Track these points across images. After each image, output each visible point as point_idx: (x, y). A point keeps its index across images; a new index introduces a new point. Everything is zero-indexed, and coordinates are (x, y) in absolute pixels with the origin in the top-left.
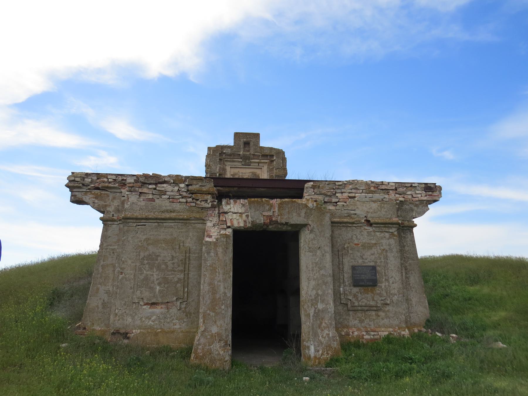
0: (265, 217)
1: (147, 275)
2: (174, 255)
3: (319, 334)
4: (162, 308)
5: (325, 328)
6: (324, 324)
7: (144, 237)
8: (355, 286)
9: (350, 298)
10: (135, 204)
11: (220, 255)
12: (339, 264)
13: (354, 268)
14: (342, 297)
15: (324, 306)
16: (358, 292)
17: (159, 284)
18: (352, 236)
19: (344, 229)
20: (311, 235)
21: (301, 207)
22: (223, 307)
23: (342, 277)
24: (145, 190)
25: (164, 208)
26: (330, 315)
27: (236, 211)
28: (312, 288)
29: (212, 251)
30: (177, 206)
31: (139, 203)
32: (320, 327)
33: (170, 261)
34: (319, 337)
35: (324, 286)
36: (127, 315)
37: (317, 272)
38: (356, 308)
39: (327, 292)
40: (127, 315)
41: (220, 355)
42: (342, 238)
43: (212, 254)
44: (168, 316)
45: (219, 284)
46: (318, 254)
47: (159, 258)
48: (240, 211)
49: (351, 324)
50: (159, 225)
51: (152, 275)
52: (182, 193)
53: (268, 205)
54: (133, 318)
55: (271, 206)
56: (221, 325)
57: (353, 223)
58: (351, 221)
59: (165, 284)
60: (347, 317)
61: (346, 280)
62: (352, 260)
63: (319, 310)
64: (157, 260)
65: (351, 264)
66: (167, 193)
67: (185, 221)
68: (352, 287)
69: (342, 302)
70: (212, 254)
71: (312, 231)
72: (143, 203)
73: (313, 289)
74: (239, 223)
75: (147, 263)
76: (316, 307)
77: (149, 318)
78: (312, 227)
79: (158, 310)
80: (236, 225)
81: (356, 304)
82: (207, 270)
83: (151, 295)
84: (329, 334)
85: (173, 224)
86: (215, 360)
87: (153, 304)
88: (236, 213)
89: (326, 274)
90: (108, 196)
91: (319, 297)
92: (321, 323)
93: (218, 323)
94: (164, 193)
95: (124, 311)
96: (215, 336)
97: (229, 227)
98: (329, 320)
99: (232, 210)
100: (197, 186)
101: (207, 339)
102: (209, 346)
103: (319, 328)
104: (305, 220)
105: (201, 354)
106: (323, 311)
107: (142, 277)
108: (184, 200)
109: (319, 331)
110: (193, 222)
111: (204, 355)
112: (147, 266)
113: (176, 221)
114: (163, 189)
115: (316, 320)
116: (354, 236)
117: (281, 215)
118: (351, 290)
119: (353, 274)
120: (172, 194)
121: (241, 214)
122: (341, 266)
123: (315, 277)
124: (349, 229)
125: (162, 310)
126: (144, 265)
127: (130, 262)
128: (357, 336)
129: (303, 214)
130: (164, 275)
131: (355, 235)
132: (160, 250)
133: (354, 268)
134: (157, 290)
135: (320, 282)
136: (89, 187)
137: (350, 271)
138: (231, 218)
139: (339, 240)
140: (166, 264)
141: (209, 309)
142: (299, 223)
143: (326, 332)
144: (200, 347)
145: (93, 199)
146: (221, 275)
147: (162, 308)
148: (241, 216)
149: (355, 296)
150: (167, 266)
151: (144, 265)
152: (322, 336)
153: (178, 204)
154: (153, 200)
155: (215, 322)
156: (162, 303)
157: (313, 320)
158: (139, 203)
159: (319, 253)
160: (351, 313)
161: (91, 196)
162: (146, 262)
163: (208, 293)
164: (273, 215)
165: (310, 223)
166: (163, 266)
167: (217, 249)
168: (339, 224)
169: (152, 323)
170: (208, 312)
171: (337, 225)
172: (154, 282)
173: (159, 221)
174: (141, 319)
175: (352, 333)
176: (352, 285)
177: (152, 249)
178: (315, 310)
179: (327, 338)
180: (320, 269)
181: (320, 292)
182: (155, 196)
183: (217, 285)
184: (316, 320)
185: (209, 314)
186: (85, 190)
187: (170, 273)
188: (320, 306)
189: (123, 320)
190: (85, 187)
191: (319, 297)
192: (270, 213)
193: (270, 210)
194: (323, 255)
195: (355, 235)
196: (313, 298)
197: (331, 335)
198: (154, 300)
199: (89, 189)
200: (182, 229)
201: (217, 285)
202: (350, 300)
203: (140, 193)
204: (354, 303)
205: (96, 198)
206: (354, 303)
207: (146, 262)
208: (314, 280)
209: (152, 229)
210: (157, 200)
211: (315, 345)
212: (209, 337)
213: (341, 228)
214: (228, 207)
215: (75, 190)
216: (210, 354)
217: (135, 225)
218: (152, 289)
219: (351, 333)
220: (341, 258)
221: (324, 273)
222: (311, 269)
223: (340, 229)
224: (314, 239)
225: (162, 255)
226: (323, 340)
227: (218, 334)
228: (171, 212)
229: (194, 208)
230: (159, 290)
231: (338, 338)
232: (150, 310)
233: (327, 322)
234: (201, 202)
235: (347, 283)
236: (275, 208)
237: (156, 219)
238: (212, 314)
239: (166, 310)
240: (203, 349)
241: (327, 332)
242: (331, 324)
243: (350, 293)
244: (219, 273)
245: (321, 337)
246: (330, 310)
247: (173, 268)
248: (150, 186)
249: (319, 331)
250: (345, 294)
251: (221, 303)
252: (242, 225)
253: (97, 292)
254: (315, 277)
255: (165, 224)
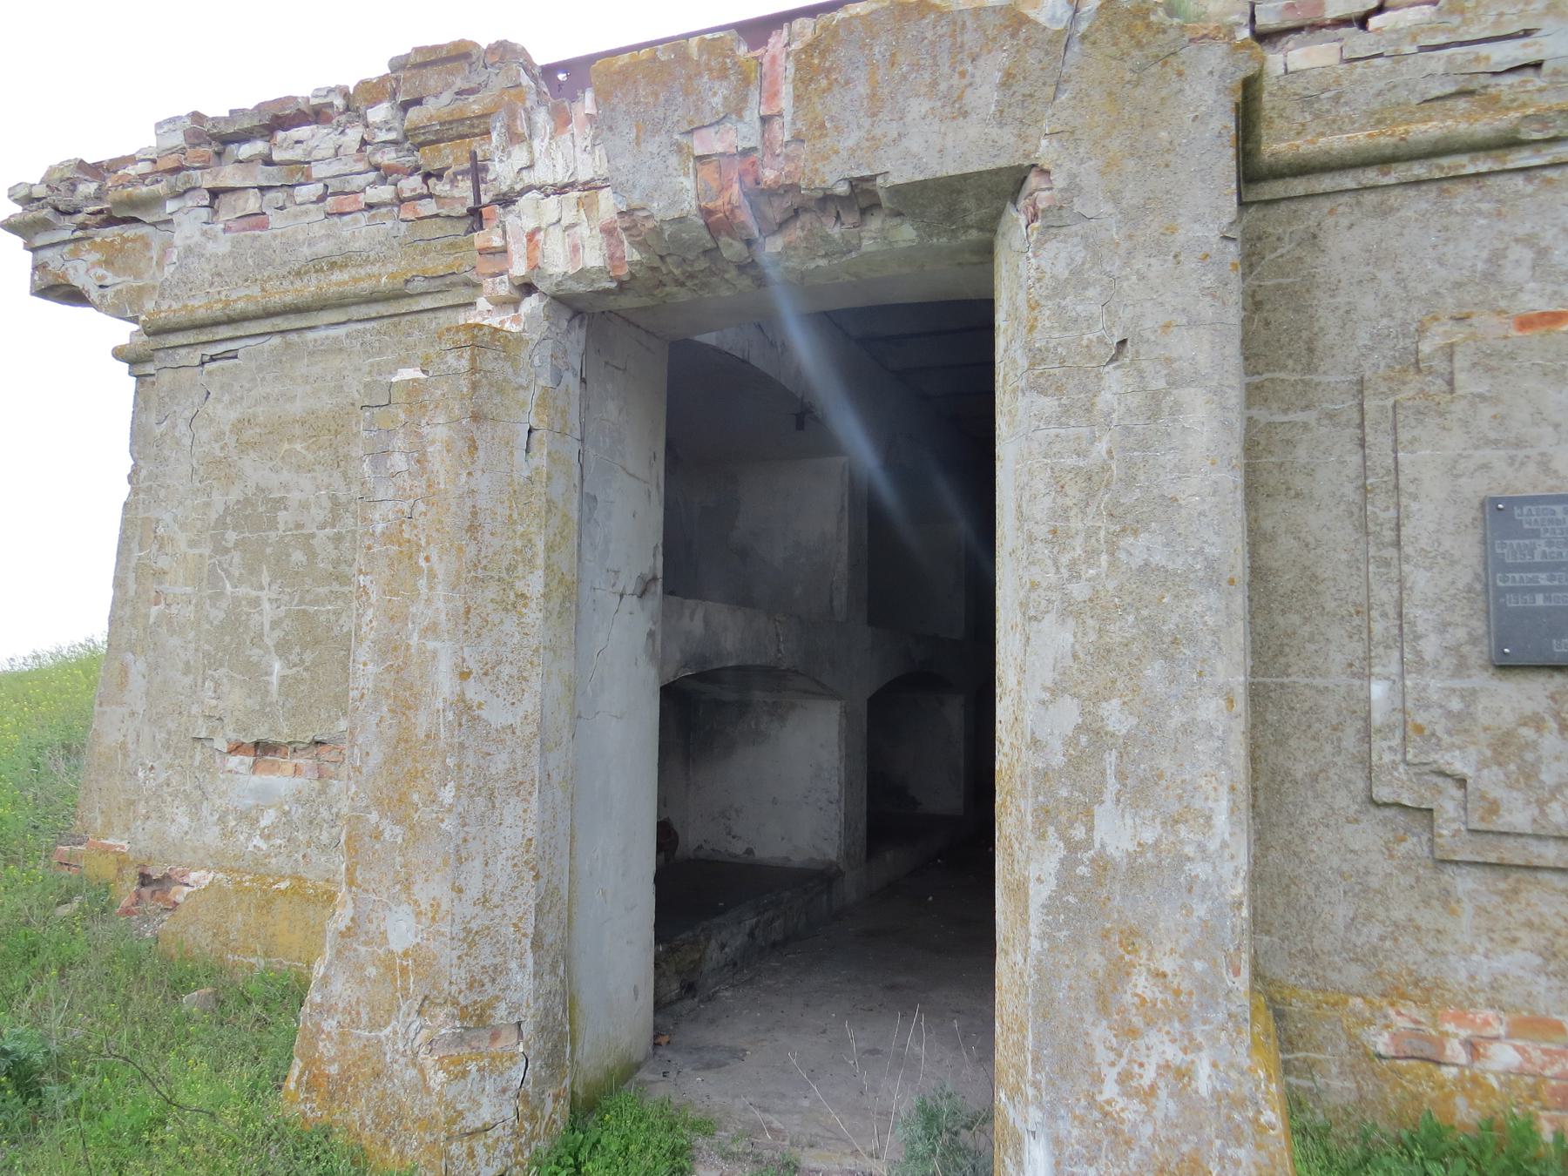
0: (708, 171)
1: (236, 602)
2: (342, 495)
3: (1102, 1055)
4: (297, 770)
5: (1152, 1014)
6: (1141, 983)
7: (233, 415)
8: (1504, 667)
9: (1459, 767)
10: (195, 250)
11: (439, 462)
12: (1364, 490)
13: (1499, 515)
14: (1384, 752)
15: (1148, 836)
16: (1537, 722)
17: (283, 648)
18: (1496, 258)
19: (1416, 204)
20: (1052, 246)
21: (969, 38)
22: (447, 795)
23: (1384, 594)
24: (228, 176)
25: (306, 251)
26: (1201, 910)
27: (562, 178)
28: (1049, 677)
29: (399, 442)
30: (359, 232)
31: (211, 247)
32: (1104, 1000)
33: (323, 527)
34: (1098, 1080)
35: (1154, 670)
36: (175, 795)
37: (1091, 555)
38: (1512, 852)
39: (1177, 718)
40: (175, 795)
41: (428, 1090)
42: (1401, 281)
43: (399, 462)
44: (324, 813)
45: (431, 645)
46: (1106, 399)
47: (282, 516)
48: (584, 175)
49: (1458, 973)
50: (288, 345)
51: (256, 603)
52: (378, 158)
53: (723, 74)
54: (195, 811)
55: (746, 81)
56: (436, 906)
57: (1511, 143)
58: (1484, 126)
59: (304, 648)
60: (1427, 918)
61: (1421, 617)
62: (1488, 454)
63: (1103, 865)
64: (273, 524)
65: (1478, 487)
66: (318, 171)
67: (388, 298)
68: (1482, 680)
69: (1383, 793)
70: (399, 462)
71: (1052, 221)
72: (222, 246)
73: (1056, 690)
74: (575, 249)
75: (236, 544)
76: (1079, 833)
77: (249, 817)
78: (1059, 180)
79: (283, 781)
80: (558, 262)
81: (1518, 816)
82: (371, 559)
83: (249, 702)
84: (1183, 1074)
85: (341, 331)
86: (400, 1117)
87: (262, 748)
88: (561, 190)
89: (1178, 565)
90: (147, 246)
91: (1111, 758)
92: (1120, 972)
93: (424, 893)
94: (300, 170)
95: (163, 776)
96: (404, 971)
97: (527, 288)
98: (1190, 953)
99: (541, 175)
100: (446, 97)
101: (362, 981)
102: (375, 1025)
103: (1104, 1009)
104: (1007, 136)
105: (333, 1069)
106: (1135, 873)
107: (218, 615)
108: (385, 192)
109: (1100, 1034)
110: (427, 303)
111: (345, 1076)
112: (237, 557)
113: (355, 312)
114: (297, 154)
115: (1077, 942)
116: (1517, 252)
117: (813, 131)
118: (1470, 696)
119: (1492, 564)
120: (336, 168)
121: (590, 186)
122: (1382, 511)
123: (1079, 591)
124: (1463, 196)
125: (299, 781)
126: (226, 551)
127: (182, 539)
128: (1510, 1077)
129: (985, 95)
130: (301, 602)
131: (1528, 241)
132: (285, 476)
133: (1499, 515)
134: (275, 679)
135: (1123, 628)
136: (80, 218)
137: (1467, 549)
138: (530, 225)
139: (1368, 304)
140: (306, 542)
141: (379, 803)
142: (951, 169)
143: (1161, 1048)
144: (330, 1025)
145: (101, 271)
146: (441, 591)
147: (297, 770)
148: (586, 205)
149: (1503, 746)
150: (312, 555)
151: (226, 551)
152: (1124, 1078)
153: (363, 218)
154: (257, 220)
155: (407, 885)
156: (295, 748)
157: (1044, 936)
158: (211, 247)
159: (1114, 387)
160: (1465, 883)
161: (95, 257)
162: (232, 536)
163: (376, 705)
164: (767, 143)
165: (1045, 151)
166: (298, 556)
167: (425, 430)
168: (1371, 176)
169: (264, 846)
170: (374, 817)
171: (1348, 181)
172: (261, 636)
173: (281, 323)
174: (222, 819)
175: (1473, 1047)
176: (1476, 655)
177: (255, 471)
178: (1068, 864)
179: (1166, 1104)
180: (1127, 522)
181: (1116, 717)
182: (270, 195)
183: (421, 652)
184: (1077, 942)
185: (377, 835)
186: (67, 235)
187: (323, 590)
188: (1117, 832)
189: (162, 818)
190: (67, 221)
191: (1111, 758)
192: (744, 134)
193: (736, 109)
194: (1154, 406)
195: (1528, 241)
196: (1058, 760)
197: (1204, 1082)
198: (261, 733)
199: (83, 226)
200: (380, 353)
201: (421, 652)
202: (1462, 782)
203: (215, 193)
204: (1493, 808)
205: (108, 263)
206: (1493, 808)
207: (232, 536)
208: (1064, 614)
209: (260, 368)
210: (275, 219)
211: (1057, 1142)
212: (372, 971)
213: (1395, 197)
214: (519, 156)
215: (40, 241)
216: (377, 1075)
217: (195, 356)
218: (254, 673)
219: (1456, 1051)
220: (1379, 442)
221: (1158, 559)
222: (1042, 531)
223: (1384, 212)
224: (1077, 279)
225: (294, 497)
226: (1130, 1111)
227: (419, 959)
228: (333, 265)
229: (431, 230)
230: (283, 678)
231: (1270, 1116)
232: (257, 780)
233: (1168, 965)
234: (453, 181)
235: (1430, 647)
236: (775, 95)
237: (269, 314)
238: (393, 832)
239: (317, 785)
240: (344, 1039)
241: (1173, 1054)
242: (1209, 991)
243: (1461, 722)
244: (432, 575)
245: (1110, 1090)
246: (1201, 870)
247: (336, 563)
248: (246, 151)
249: (1100, 1034)
250: (1409, 731)
251: (436, 766)
252: (593, 258)
253: (122, 685)
254: (1079, 591)
255: (310, 335)
